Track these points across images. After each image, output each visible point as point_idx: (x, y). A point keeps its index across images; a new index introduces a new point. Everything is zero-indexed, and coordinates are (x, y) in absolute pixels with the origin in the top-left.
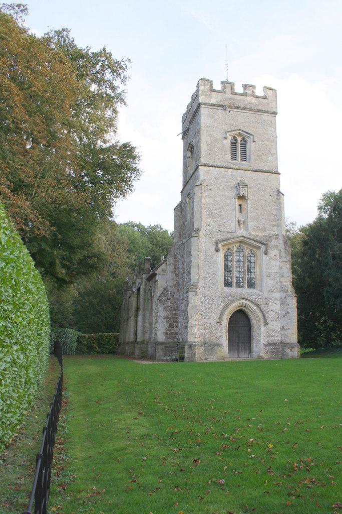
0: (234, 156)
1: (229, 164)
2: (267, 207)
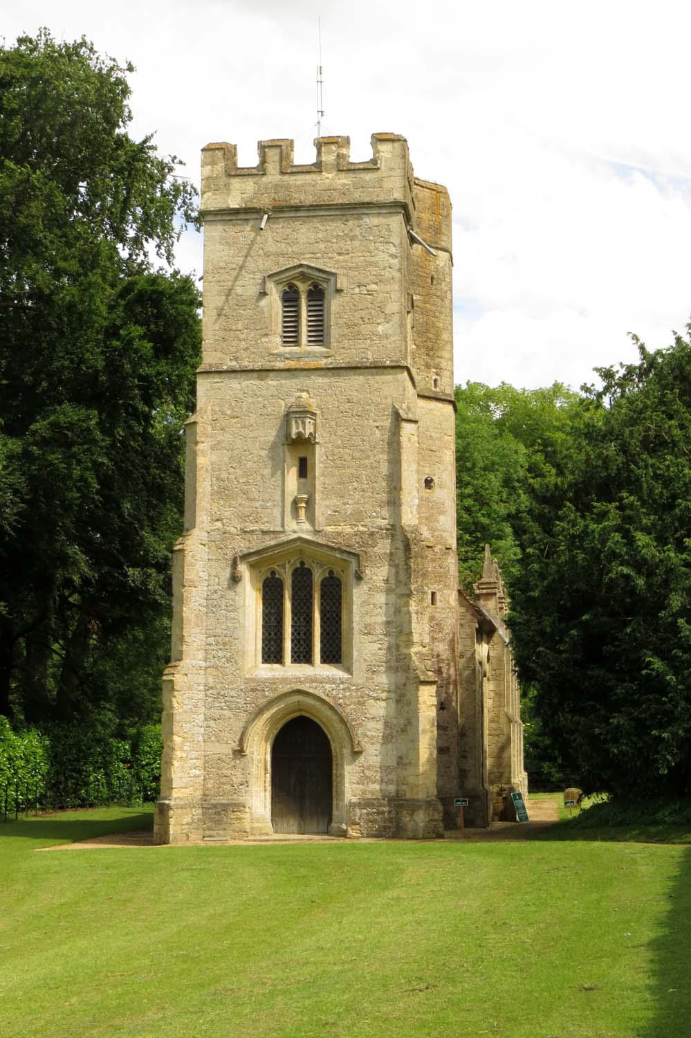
0: (292, 337)
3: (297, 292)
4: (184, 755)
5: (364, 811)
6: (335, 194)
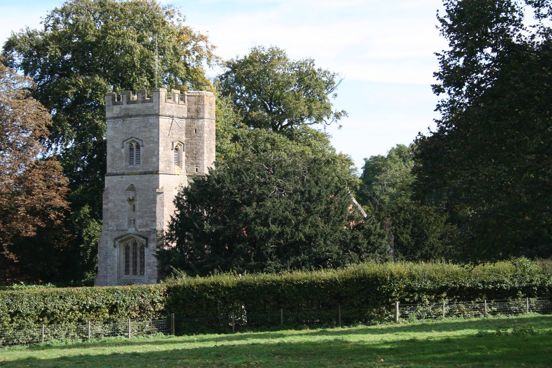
1: (125, 170)
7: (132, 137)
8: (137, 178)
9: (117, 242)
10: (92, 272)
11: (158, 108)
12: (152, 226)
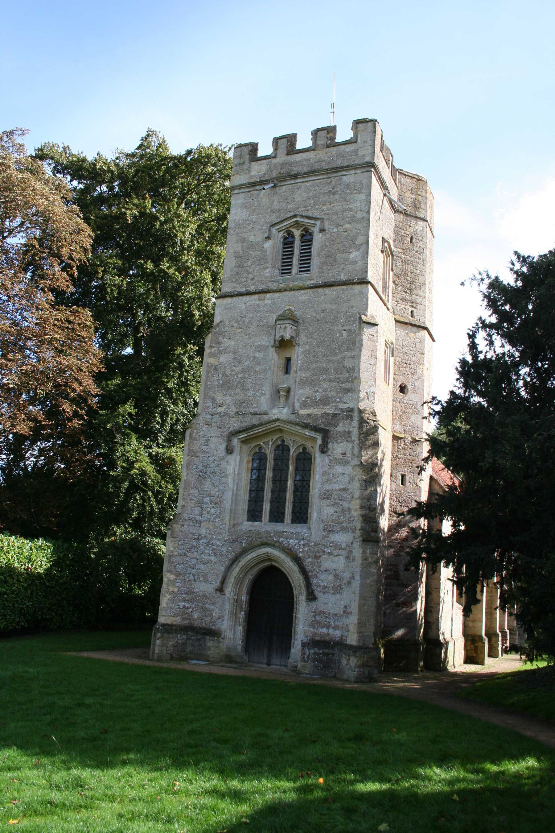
0: (286, 268)
1: (270, 284)
2: (335, 354)
3: (293, 237)
4: (176, 590)
5: (312, 651)
6: (323, 163)
7: (295, 216)
8: (303, 296)
9: (235, 441)
10: (125, 526)
11: (370, 151)
12: (341, 402)
